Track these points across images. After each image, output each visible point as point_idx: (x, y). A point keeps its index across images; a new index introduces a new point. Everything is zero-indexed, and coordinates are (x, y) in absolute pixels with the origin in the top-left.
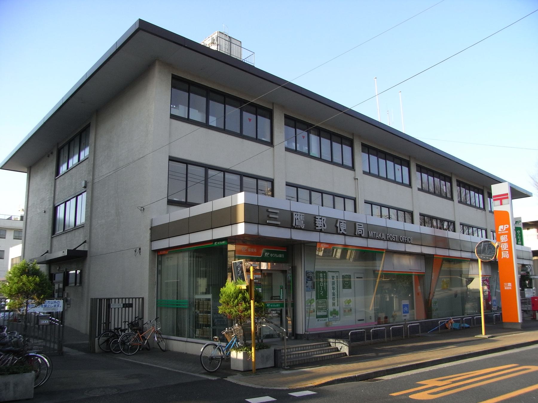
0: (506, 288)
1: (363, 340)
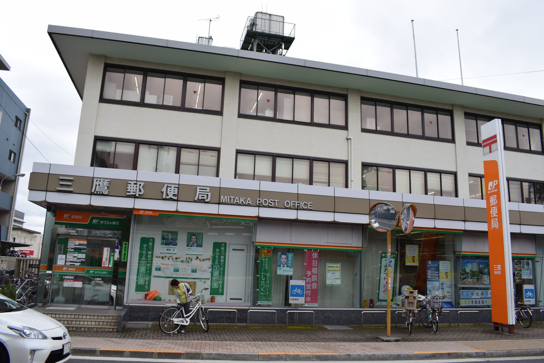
0: (495, 272)
1: (235, 323)
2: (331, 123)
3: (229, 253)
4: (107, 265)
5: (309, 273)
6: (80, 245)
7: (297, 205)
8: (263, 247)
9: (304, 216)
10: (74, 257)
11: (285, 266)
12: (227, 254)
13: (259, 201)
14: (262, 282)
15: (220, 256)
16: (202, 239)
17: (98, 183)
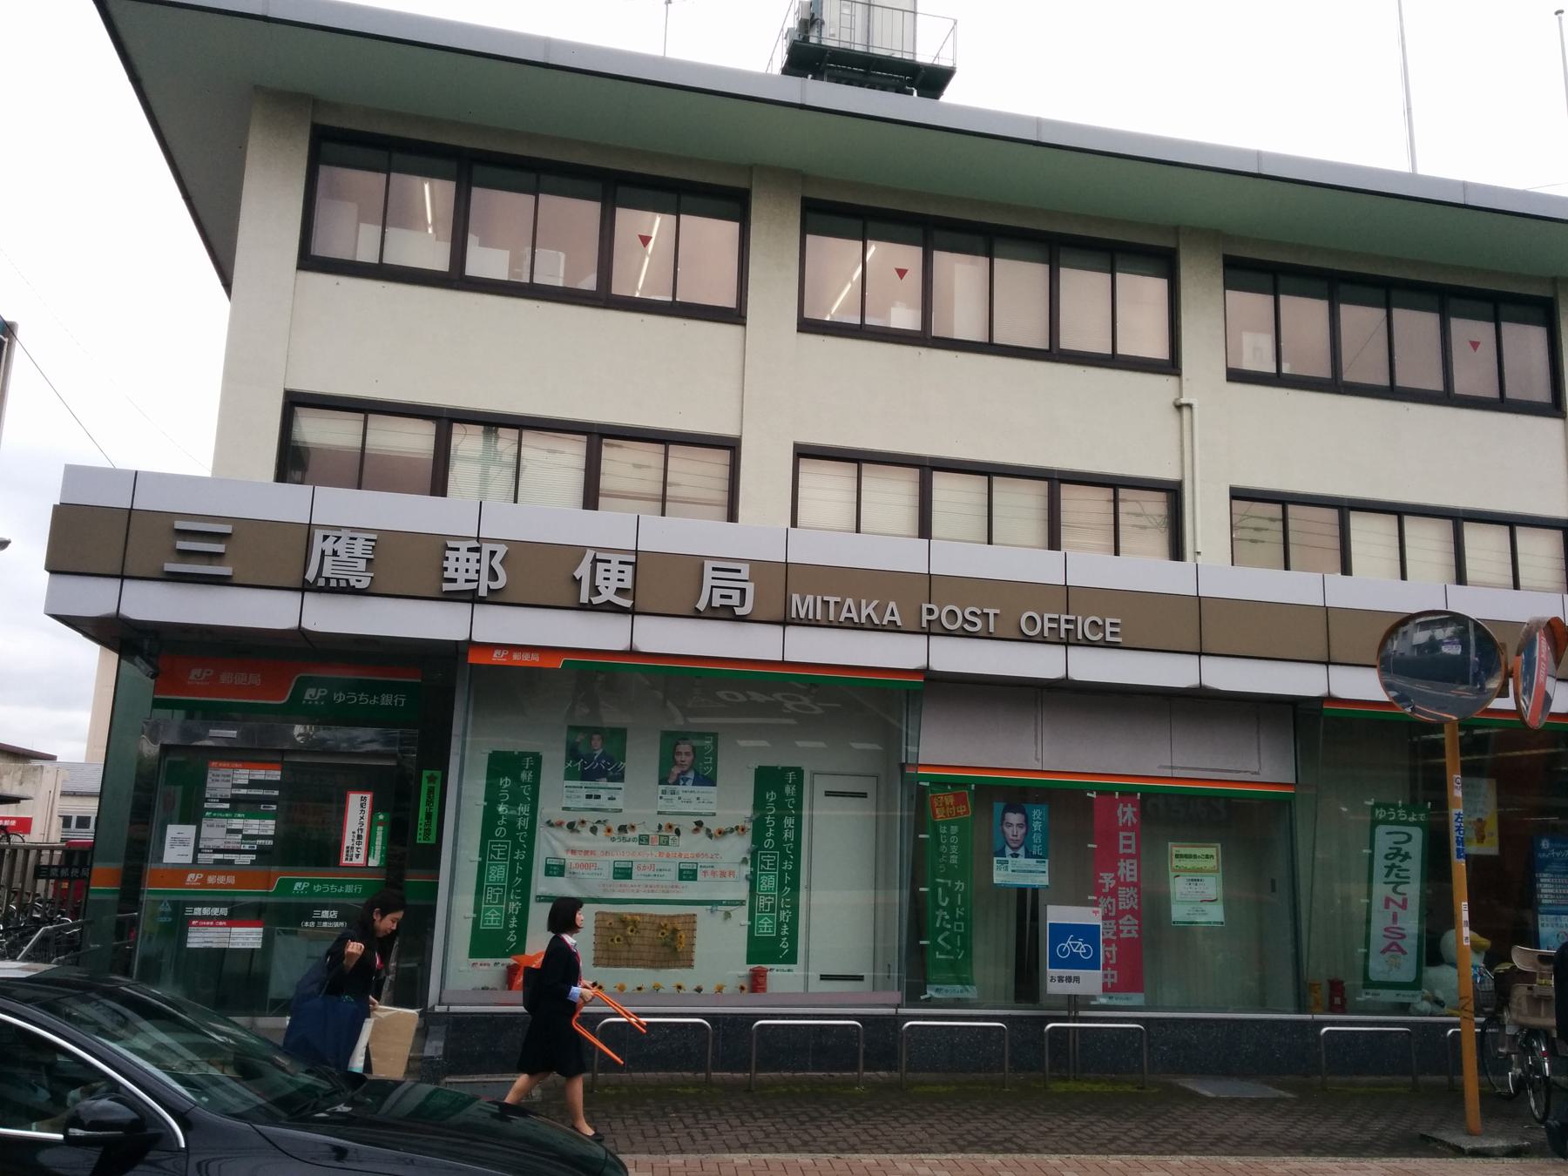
1: (853, 1067)
2: (1120, 351)
3: (811, 808)
4: (360, 861)
5: (1107, 879)
6: (253, 784)
7: (1064, 626)
8: (940, 783)
9: (1091, 666)
10: (230, 831)
11: (1021, 851)
12: (805, 813)
13: (930, 612)
14: (940, 913)
15: (779, 819)
16: (715, 755)
17: (328, 546)
